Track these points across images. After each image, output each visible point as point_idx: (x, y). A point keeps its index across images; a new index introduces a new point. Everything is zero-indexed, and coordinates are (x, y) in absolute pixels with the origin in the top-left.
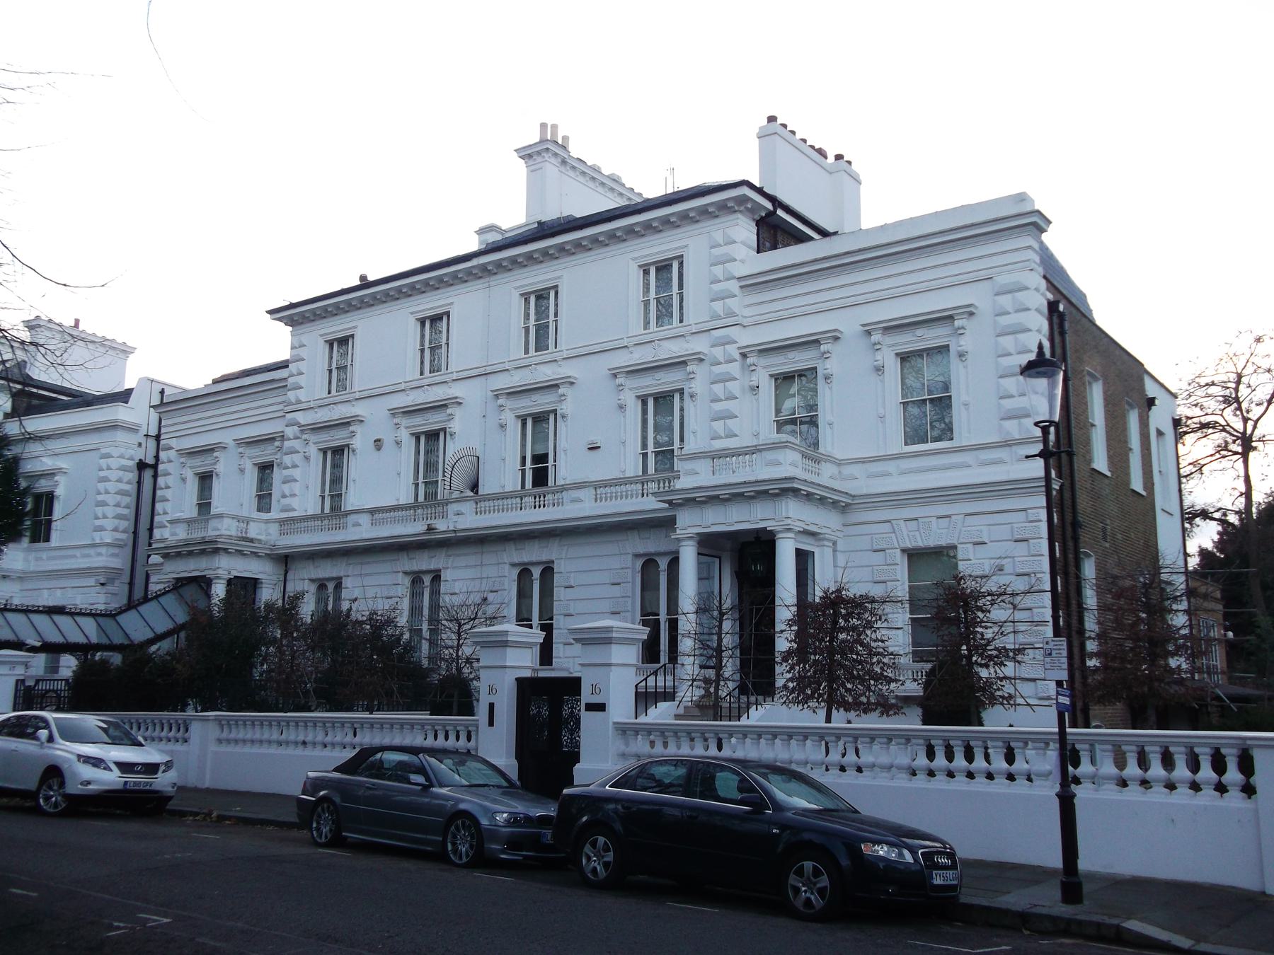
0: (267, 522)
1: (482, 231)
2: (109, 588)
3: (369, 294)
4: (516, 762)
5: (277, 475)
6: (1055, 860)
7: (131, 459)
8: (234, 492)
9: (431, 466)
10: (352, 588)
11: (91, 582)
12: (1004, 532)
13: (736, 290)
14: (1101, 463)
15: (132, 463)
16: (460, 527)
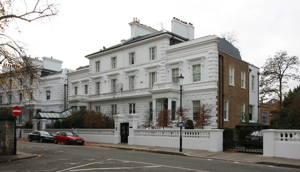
0: (87, 96)
1: (121, 41)
2: (61, 108)
3: (105, 52)
4: (120, 136)
5: (88, 87)
6: (179, 147)
7: (63, 84)
8: (81, 91)
9: (114, 85)
10: (102, 108)
11: (58, 107)
12: (207, 98)
13: (165, 53)
14: (232, 83)
15: (63, 85)
16: (119, 97)
